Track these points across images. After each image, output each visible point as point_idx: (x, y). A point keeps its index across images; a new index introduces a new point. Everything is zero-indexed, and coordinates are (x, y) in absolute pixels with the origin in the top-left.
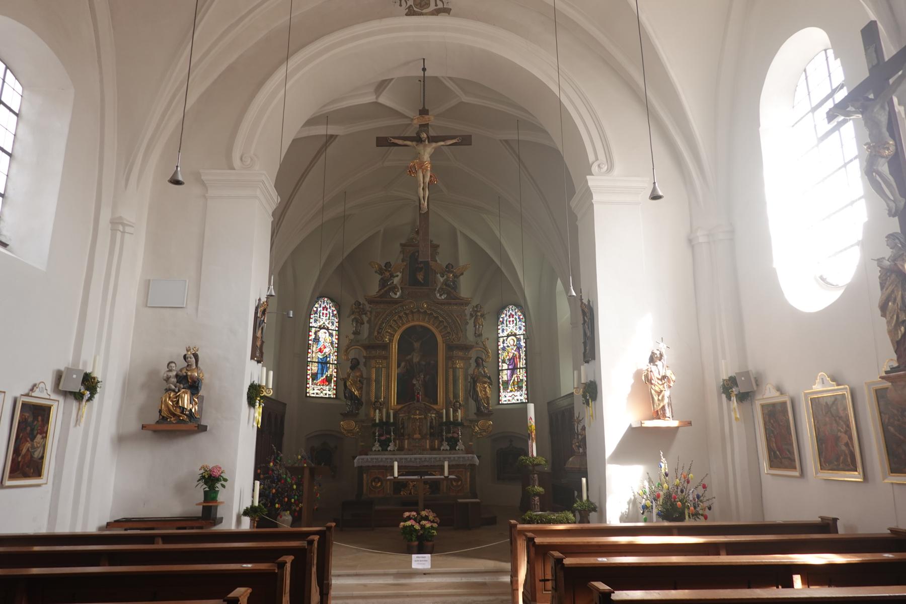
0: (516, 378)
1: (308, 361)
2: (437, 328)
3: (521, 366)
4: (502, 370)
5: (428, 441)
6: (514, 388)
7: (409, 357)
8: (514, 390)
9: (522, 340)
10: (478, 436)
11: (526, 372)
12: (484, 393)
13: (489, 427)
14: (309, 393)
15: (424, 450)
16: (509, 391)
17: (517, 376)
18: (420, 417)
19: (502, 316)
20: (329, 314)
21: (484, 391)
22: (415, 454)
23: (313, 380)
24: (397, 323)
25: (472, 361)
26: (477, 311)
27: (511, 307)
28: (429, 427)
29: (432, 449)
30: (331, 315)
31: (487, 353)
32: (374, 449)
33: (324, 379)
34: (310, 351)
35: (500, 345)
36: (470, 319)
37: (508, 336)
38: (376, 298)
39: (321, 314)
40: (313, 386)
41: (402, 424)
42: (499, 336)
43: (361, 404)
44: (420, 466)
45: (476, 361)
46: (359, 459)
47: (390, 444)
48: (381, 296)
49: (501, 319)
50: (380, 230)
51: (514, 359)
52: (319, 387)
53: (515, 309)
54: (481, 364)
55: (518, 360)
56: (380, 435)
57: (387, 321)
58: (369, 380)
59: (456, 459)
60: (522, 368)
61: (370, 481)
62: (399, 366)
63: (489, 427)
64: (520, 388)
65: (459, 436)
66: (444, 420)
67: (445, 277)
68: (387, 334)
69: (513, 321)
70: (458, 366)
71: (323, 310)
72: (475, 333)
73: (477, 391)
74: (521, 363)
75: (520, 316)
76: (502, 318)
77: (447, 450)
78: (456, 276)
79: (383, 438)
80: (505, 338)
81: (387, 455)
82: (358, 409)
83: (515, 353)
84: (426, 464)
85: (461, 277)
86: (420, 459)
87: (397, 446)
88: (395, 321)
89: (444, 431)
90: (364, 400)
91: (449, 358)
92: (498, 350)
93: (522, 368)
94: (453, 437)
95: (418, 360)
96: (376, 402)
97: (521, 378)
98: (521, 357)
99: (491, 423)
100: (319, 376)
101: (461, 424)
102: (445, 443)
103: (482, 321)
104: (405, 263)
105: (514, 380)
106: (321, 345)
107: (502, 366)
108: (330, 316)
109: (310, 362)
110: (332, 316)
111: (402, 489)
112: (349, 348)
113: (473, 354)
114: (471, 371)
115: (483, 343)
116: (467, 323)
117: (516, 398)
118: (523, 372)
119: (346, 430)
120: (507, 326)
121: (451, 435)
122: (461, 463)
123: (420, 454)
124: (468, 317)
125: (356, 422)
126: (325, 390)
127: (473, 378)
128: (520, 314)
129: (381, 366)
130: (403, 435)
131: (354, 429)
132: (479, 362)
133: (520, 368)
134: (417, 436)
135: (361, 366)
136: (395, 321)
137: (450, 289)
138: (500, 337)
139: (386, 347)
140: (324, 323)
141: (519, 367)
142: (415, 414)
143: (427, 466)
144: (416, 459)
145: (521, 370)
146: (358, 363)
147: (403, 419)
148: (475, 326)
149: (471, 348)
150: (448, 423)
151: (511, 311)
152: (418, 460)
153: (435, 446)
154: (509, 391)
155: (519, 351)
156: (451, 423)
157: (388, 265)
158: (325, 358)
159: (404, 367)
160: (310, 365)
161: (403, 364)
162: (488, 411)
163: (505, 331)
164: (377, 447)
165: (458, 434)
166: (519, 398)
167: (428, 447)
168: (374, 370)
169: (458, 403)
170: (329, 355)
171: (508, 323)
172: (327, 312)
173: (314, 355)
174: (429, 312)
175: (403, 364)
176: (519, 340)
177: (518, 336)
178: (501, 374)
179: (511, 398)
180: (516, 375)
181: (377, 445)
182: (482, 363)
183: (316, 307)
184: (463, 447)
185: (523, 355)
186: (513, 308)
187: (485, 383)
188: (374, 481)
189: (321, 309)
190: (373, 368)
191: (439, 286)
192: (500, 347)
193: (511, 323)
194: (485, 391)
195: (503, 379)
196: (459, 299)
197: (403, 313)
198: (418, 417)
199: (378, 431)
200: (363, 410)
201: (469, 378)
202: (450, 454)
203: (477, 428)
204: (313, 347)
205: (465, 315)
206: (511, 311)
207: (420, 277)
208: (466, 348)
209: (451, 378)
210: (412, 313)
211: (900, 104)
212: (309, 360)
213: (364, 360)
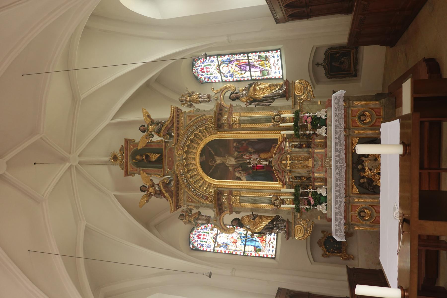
0: (258, 63)
1: (244, 255)
2: (201, 140)
3: (246, 58)
4: (251, 77)
5: (316, 151)
6: (267, 64)
7: (230, 168)
8: (269, 64)
9: (223, 58)
10: (311, 94)
11: (252, 53)
12: (265, 90)
13: (302, 84)
14: (272, 256)
15: (326, 155)
16: (270, 69)
17: (256, 62)
18: (289, 159)
19: (204, 79)
20: (204, 232)
21: (263, 90)
22: (331, 165)
23: (260, 251)
24: (197, 181)
25: (234, 103)
26: (186, 101)
27: (194, 71)
28: (301, 150)
29: (325, 145)
30: (205, 231)
31: (226, 88)
32: (324, 212)
33: (260, 240)
34: (234, 253)
35: (229, 80)
36: (194, 107)
37: (220, 72)
38: (173, 201)
39: (204, 240)
40: (266, 251)
41: (297, 179)
42: (221, 81)
43: (278, 217)
44: (346, 162)
45: (234, 99)
46: (336, 235)
47: (319, 193)
48: (171, 196)
49: (206, 80)
50: (115, 195)
51: (240, 66)
52: (268, 245)
53: (196, 67)
54: (236, 94)
55: (241, 61)
56: (309, 204)
57: (195, 190)
58: (252, 210)
59: (337, 118)
60: (248, 57)
61: (364, 223)
62: (239, 179)
63: (302, 84)
64: (267, 58)
65: (310, 116)
66: (292, 132)
67: (153, 133)
68: (208, 189)
69: (207, 68)
70: (238, 118)
71: (200, 238)
72: (207, 101)
73: (263, 97)
74: (243, 58)
75: (201, 62)
76: (205, 79)
77: (326, 129)
78: (151, 122)
79: (312, 201)
80: (222, 75)
81: (331, 151)
82: (283, 220)
83: (234, 65)
84: (343, 155)
85: (152, 117)
86: (337, 162)
87: (321, 184)
88: (195, 182)
89: (304, 132)
90: (274, 215)
91: (231, 128)
92: (233, 81)
93: (248, 57)
94: (312, 123)
95: (233, 159)
96: (274, 204)
97: (257, 58)
98: (238, 58)
99: (297, 81)
100: (257, 244)
101: (297, 114)
102: (319, 131)
103: (195, 96)
104: (141, 172)
105: (259, 64)
106: (229, 241)
107: (248, 77)
108: (206, 233)
109: (244, 253)
110: (206, 229)
111: (374, 184)
112: (223, 228)
113: (227, 103)
114: (243, 105)
115: (216, 94)
116: (198, 110)
117: (276, 62)
118: (252, 56)
119: (304, 235)
120: (211, 74)
121: (309, 125)
122: (343, 112)
123: (331, 160)
124: (192, 109)
125: (296, 224)
126: (270, 239)
127: (251, 103)
128: (200, 62)
129: (238, 198)
130: (309, 178)
131: (303, 226)
132: (235, 97)
133: (248, 59)
134: (310, 163)
135: (239, 216)
136: (195, 182)
137: (163, 128)
138: (222, 80)
139: (219, 193)
140: (211, 238)
141: (247, 61)
142: (286, 165)
143: (345, 154)
144: (337, 168)
145: (250, 58)
146: (236, 220)
147: (291, 178)
148: (200, 102)
149: (221, 104)
150: (296, 128)
151: (198, 71)
152: (339, 165)
153: (321, 142)
154: (270, 69)
155: (232, 61)
156: (296, 125)
157: (143, 189)
158: (242, 238)
159: (240, 173)
160: (247, 253)
161: (237, 175)
162: (285, 85)
163: (216, 76)
164: (322, 208)
165: (308, 117)
166: (276, 58)
167: (322, 151)
168: (243, 204)
169: (276, 117)
170: (239, 234)
171: (209, 73)
172: (202, 235)
173: (238, 249)
174: (186, 149)
175: (237, 175)
176: (223, 62)
177: (220, 63)
178: (255, 78)
179: (277, 67)
180: (255, 63)
181: (320, 207)
182: (235, 93)
183: (198, 245)
184: (323, 111)
185: (236, 57)
186: (196, 69)
187: (254, 90)
188: (363, 217)
189: (199, 240)
190: (240, 206)
191: (162, 138)
192: (231, 80)
193: (208, 70)
194: (263, 89)
195: (260, 75)
196: (172, 120)
197: (188, 175)
198: (289, 162)
199: (305, 205)
200: (284, 216)
201: (250, 106)
202: (331, 125)
203: (302, 97)
204: (231, 249)
205: (190, 112)
206: (198, 71)
207: (154, 157)
208: (220, 110)
209: (250, 125)
210: (187, 165)
211: (354, 150)
212: (242, 254)
213: (234, 213)
